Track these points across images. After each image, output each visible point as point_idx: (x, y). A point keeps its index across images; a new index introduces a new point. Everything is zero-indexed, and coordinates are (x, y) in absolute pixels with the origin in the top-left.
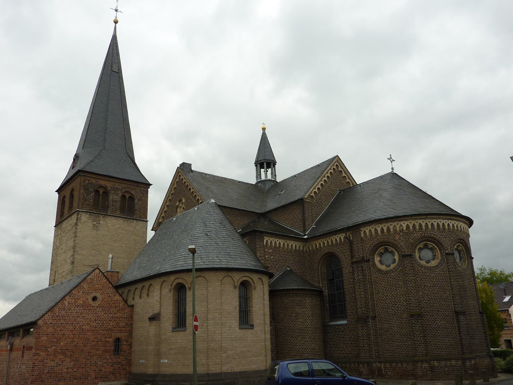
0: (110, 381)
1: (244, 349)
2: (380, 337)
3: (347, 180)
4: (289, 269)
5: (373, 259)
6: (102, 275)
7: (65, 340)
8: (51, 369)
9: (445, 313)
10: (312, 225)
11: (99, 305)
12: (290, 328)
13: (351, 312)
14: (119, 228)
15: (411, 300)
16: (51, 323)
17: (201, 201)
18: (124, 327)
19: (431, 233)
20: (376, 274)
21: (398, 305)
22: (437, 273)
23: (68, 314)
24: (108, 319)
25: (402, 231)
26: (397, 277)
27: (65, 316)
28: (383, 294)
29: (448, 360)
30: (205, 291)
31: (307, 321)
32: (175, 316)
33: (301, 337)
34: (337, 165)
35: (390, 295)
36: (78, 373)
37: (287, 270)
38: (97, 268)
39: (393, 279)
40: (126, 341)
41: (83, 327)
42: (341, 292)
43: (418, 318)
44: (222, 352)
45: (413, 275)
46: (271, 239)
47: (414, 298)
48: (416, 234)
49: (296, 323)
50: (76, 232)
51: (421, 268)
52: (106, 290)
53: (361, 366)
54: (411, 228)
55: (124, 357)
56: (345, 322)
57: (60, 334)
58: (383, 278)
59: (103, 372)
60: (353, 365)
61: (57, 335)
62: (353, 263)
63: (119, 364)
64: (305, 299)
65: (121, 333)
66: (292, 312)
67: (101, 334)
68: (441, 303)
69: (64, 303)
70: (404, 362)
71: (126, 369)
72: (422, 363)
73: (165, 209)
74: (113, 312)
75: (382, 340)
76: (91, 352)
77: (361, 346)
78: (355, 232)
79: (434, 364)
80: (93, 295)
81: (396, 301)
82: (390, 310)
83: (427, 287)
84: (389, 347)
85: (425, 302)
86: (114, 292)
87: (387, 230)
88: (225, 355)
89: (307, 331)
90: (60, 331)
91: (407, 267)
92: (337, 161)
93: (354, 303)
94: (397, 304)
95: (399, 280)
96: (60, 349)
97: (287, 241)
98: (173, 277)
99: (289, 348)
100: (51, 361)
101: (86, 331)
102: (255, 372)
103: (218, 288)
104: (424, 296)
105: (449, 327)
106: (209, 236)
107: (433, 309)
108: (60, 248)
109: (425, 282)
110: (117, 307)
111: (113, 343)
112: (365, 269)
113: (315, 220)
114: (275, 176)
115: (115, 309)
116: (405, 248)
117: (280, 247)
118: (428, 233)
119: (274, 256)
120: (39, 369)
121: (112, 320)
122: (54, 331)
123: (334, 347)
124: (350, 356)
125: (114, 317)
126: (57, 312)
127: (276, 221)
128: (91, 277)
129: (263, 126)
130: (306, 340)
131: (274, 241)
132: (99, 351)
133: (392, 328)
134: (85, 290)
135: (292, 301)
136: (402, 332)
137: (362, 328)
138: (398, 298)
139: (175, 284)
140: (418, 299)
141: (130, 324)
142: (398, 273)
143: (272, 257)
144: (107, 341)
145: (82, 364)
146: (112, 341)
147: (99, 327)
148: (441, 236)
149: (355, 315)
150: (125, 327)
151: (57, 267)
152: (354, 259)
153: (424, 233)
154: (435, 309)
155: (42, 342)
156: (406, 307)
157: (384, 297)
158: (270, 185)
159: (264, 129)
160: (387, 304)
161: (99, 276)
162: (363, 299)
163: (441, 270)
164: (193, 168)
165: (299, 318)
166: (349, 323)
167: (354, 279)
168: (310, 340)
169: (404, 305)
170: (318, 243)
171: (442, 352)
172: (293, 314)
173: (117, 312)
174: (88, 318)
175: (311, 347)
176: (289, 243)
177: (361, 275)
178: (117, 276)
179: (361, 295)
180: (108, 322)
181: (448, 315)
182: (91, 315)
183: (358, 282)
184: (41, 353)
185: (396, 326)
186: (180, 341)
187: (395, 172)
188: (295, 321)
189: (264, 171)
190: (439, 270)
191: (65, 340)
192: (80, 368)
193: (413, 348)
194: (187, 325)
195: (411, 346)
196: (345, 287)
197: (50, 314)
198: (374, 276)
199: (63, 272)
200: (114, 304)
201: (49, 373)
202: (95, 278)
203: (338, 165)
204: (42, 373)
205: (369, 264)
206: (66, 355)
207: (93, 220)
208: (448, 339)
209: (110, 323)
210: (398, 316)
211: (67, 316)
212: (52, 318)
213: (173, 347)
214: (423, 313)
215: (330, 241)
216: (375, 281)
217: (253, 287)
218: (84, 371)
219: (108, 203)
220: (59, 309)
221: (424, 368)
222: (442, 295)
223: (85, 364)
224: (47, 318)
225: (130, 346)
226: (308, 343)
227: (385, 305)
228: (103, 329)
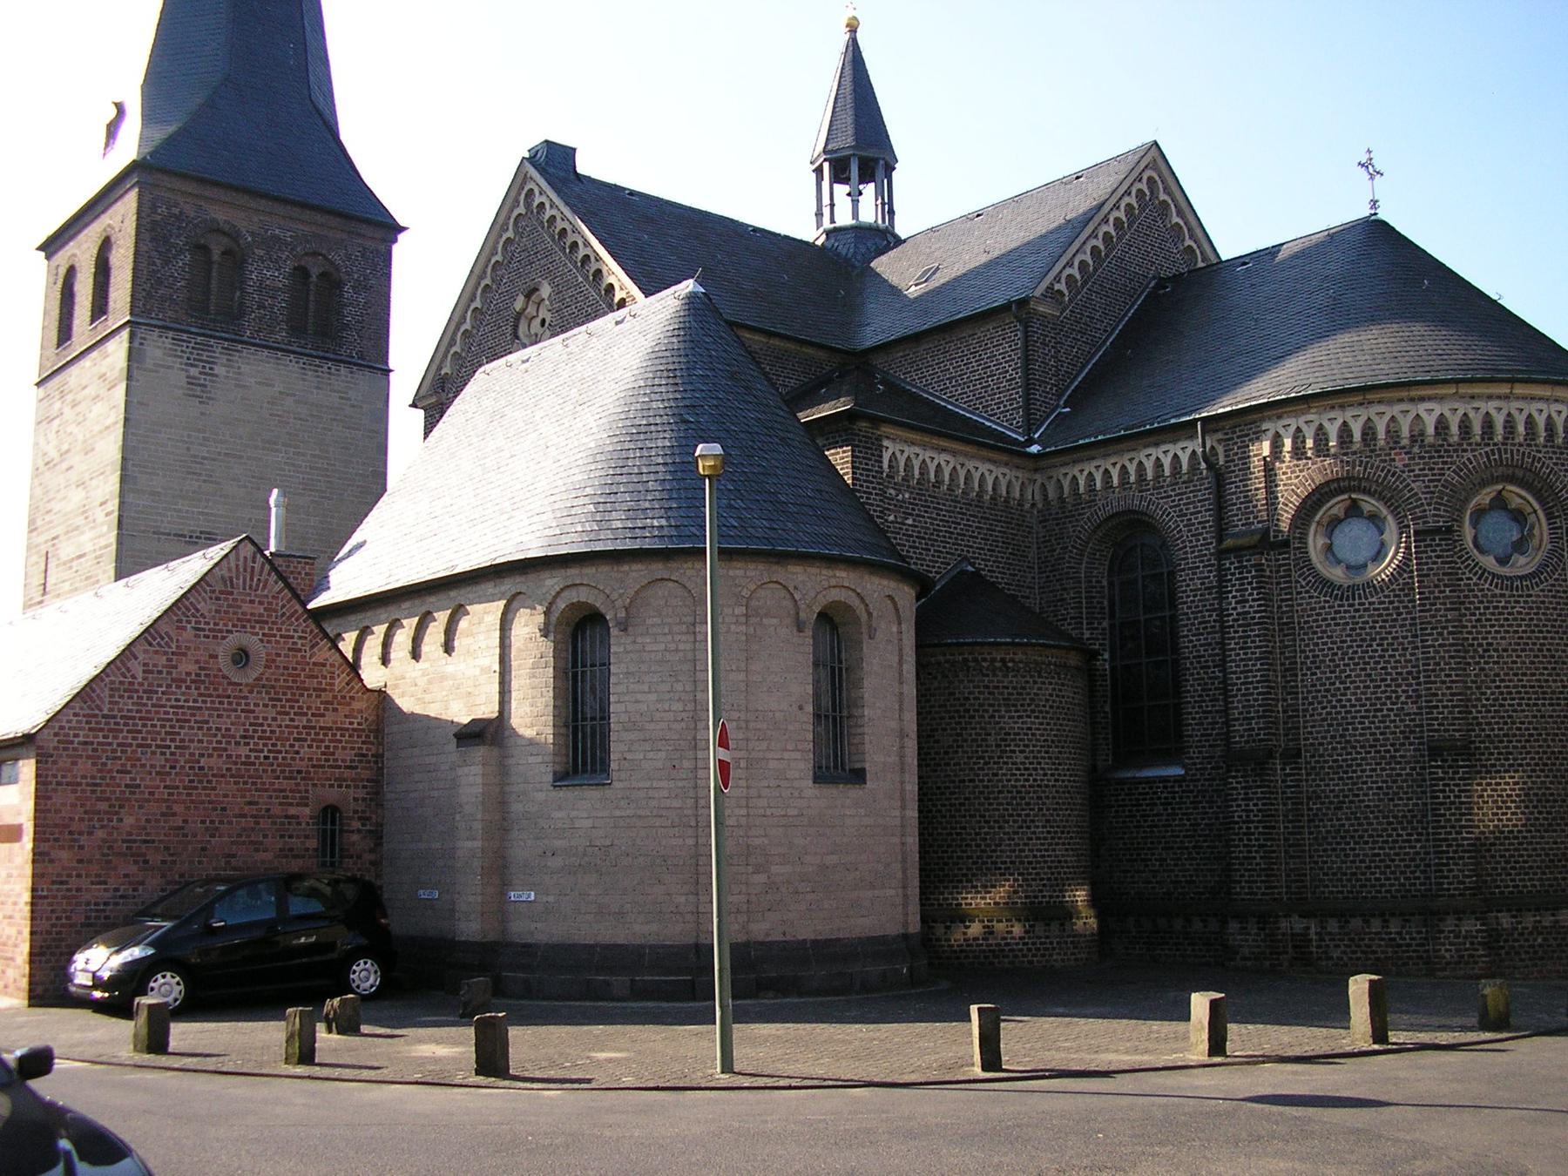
1: (832, 860)
2: (1309, 827)
3: (1183, 240)
4: (970, 568)
5: (1303, 539)
6: (263, 564)
7: (141, 807)
8: (97, 911)
9: (1549, 747)
10: (1058, 406)
12: (977, 787)
13: (1202, 735)
15: (1437, 695)
16: (86, 743)
19: (1524, 453)
20: (1310, 597)
21: (1385, 712)
22: (1533, 602)
23: (147, 712)
25: (1417, 437)
26: (1388, 609)
27: (133, 718)
28: (1331, 672)
29: (1547, 909)
30: (684, 638)
31: (1040, 763)
32: (563, 731)
34: (1150, 179)
35: (1360, 676)
37: (963, 572)
39: (1373, 615)
40: (360, 818)
42: (1140, 664)
43: (1457, 760)
44: (750, 869)
45: (1451, 603)
46: (910, 450)
47: (1448, 688)
48: (1470, 455)
51: (1479, 579)
52: (283, 624)
53: (1234, 926)
54: (1454, 429)
56: (1178, 771)
58: (1336, 612)
60: (1197, 925)
61: (108, 789)
62: (1222, 554)
64: (1035, 682)
65: (340, 786)
66: (985, 729)
67: (266, 790)
68: (1540, 711)
69: (128, 670)
70: (1393, 915)
72: (1459, 919)
73: (467, 326)
74: (309, 708)
75: (1316, 839)
76: (234, 856)
77: (1237, 858)
78: (1238, 437)
79: (1498, 924)
80: (235, 639)
81: (1380, 698)
82: (1357, 729)
83: (1496, 650)
84: (1343, 862)
85: (1484, 706)
86: (311, 631)
87: (1364, 434)
88: (761, 878)
89: (1040, 798)
90: (118, 772)
91: (1428, 575)
92: (1152, 165)
93: (1217, 700)
94: (1382, 710)
95: (1396, 620)
96: (124, 841)
97: (967, 463)
98: (555, 580)
99: (971, 857)
100: (92, 883)
101: (213, 775)
103: (733, 627)
104: (1482, 681)
105: (1559, 795)
106: (693, 426)
107: (1511, 729)
109: (1490, 632)
110: (325, 690)
112: (1269, 577)
113: (1068, 387)
114: (892, 212)
115: (318, 696)
116: (1429, 504)
117: (939, 482)
118: (1512, 451)
119: (918, 515)
121: (306, 740)
123: (1128, 860)
125: (314, 728)
126: (103, 702)
127: (909, 384)
128: (225, 572)
129: (851, 13)
131: (921, 458)
132: (265, 850)
133: (1358, 795)
134: (206, 623)
136: (1392, 811)
137: (1246, 794)
138: (1389, 686)
139: (563, 606)
140: (1459, 694)
142: (1395, 596)
143: (910, 522)
144: (292, 817)
146: (311, 818)
148: (1556, 464)
150: (357, 767)
153: (1499, 450)
154: (1520, 729)
155: (58, 811)
156: (1414, 720)
157: (1334, 684)
159: (853, 28)
160: (1345, 706)
162: (1257, 688)
163: (1550, 591)
164: (583, 167)
165: (1014, 752)
166: (1193, 775)
167: (1222, 613)
168: (1049, 832)
169: (1409, 714)
170: (1086, 473)
171: (1530, 880)
173: (326, 709)
174: (218, 729)
176: (973, 471)
177: (1254, 600)
178: (306, 574)
179: (1251, 671)
180: (292, 746)
181: (1560, 753)
182: (229, 717)
183: (1239, 626)
185: (1372, 788)
186: (589, 823)
187: (1382, 215)
189: (849, 194)
190: (1542, 590)
191: (141, 807)
193: (1429, 865)
194: (613, 766)
195: (1422, 860)
196: (1183, 642)
197: (82, 709)
198: (1301, 605)
202: (238, 579)
203: (1157, 178)
205: (1284, 559)
208: (1552, 837)
210: (1386, 751)
212: (87, 723)
213: (558, 843)
214: (1474, 742)
215: (1132, 469)
216: (1306, 622)
217: (864, 630)
219: (242, 297)
220: (112, 689)
221: (1465, 937)
222: (1547, 681)
225: (377, 836)
226: (1042, 844)
227: (1337, 713)
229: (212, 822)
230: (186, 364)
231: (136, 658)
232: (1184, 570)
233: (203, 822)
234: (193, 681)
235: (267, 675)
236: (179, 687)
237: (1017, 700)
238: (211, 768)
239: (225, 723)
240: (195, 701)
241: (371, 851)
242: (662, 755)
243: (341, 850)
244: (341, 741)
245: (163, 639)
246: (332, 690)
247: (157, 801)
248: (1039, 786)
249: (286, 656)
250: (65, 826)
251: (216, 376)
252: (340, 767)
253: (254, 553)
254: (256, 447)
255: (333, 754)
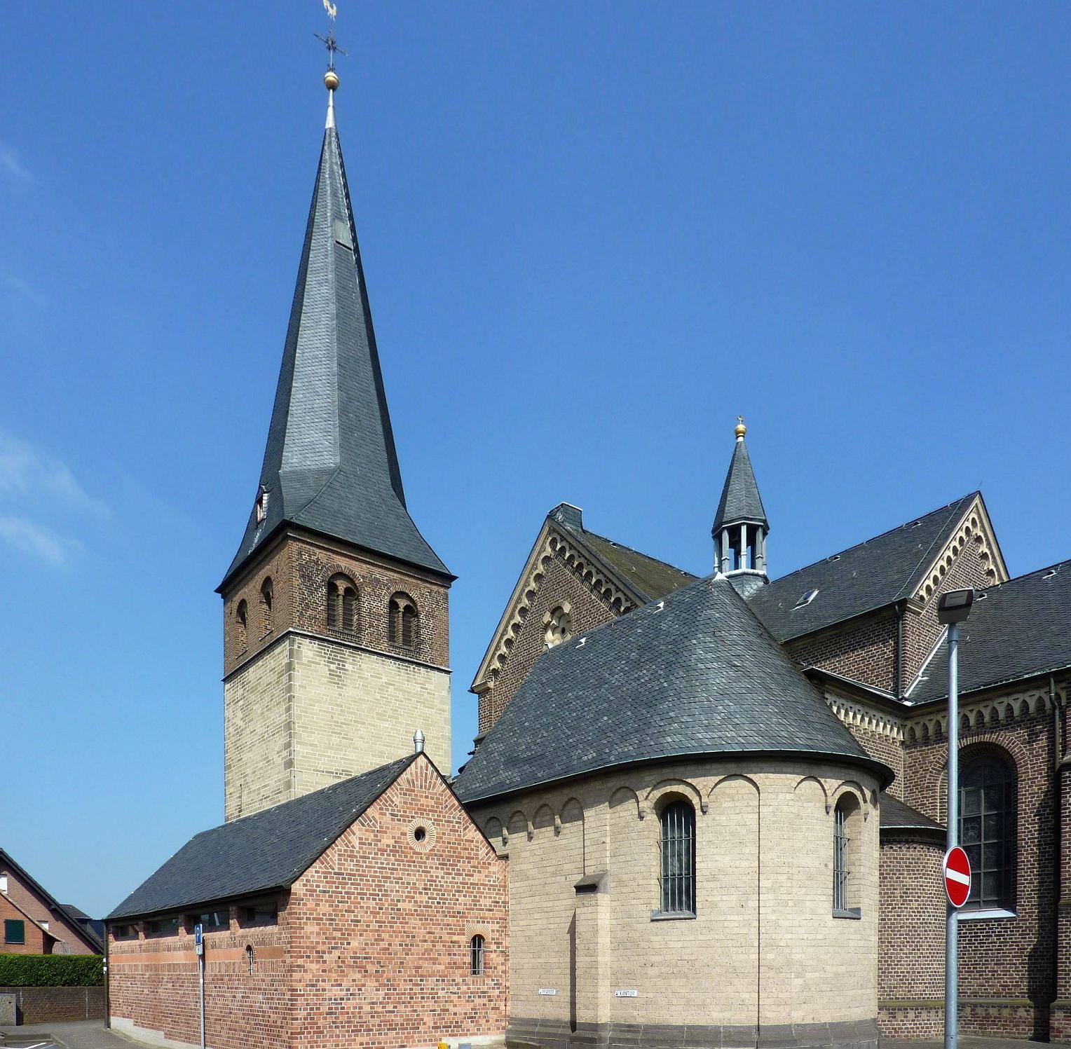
0: (466, 1035)
1: (842, 969)
7: (361, 935)
8: (336, 1004)
11: (432, 850)
14: (391, 685)
16: (324, 892)
17: (628, 604)
18: (490, 910)
24: (453, 887)
27: (354, 875)
31: (926, 908)
33: (911, 946)
36: (396, 1016)
38: (422, 753)
41: (400, 905)
49: (903, 912)
50: (289, 689)
55: (493, 980)
57: (347, 921)
59: (450, 1014)
63: (484, 997)
64: (926, 856)
65: (483, 922)
67: (439, 925)
69: (350, 843)
71: (498, 1009)
86: (464, 818)
88: (800, 981)
96: (351, 958)
98: (652, 777)
101: (406, 914)
102: (860, 1023)
108: (248, 731)
110: (473, 858)
111: (468, 947)
115: (469, 862)
120: (307, 1004)
121: (462, 892)
122: (334, 910)
124: (1015, 993)
130: (922, 953)
132: (440, 964)
135: (896, 858)
141: (503, 902)
145: (404, 994)
147: (435, 907)
149: (1046, 897)
151: (244, 777)
152: (1069, 757)
155: (308, 937)
158: (755, 587)
161: (426, 774)
165: (912, 901)
168: (930, 953)
172: (896, 889)
175: (930, 968)
180: (454, 895)
182: (415, 875)
184: (308, 966)
186: (679, 945)
188: (899, 908)
192: (399, 1003)
197: (320, 868)
199: (265, 786)
200: (465, 849)
201: (331, 1013)
204: (314, 1014)
206: (366, 971)
207: (329, 658)
209: (460, 898)
211: (359, 875)
218: (410, 1011)
223: (410, 994)
224: (313, 876)
226: (926, 961)
228: (443, 912)
229: (406, 945)
230: (328, 662)
231: (354, 834)
232: (1025, 780)
233: (401, 945)
234: (391, 851)
235: (438, 847)
236: (382, 855)
237: (915, 867)
238: (405, 910)
239: (413, 879)
240: (393, 864)
241: (503, 964)
242: (735, 898)
243: (485, 964)
244: (483, 893)
245: (371, 821)
246: (477, 858)
247: (372, 931)
248: (926, 923)
249: (449, 835)
250: (314, 948)
251: (347, 670)
252: (483, 910)
253: (427, 764)
254: (373, 717)
255: (479, 901)
